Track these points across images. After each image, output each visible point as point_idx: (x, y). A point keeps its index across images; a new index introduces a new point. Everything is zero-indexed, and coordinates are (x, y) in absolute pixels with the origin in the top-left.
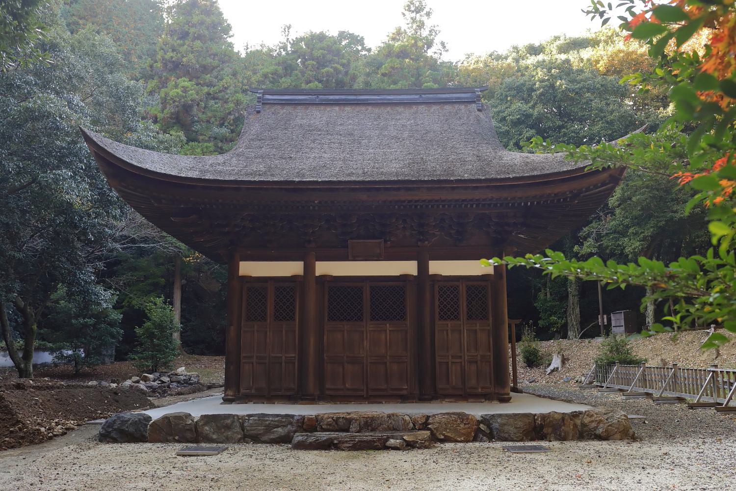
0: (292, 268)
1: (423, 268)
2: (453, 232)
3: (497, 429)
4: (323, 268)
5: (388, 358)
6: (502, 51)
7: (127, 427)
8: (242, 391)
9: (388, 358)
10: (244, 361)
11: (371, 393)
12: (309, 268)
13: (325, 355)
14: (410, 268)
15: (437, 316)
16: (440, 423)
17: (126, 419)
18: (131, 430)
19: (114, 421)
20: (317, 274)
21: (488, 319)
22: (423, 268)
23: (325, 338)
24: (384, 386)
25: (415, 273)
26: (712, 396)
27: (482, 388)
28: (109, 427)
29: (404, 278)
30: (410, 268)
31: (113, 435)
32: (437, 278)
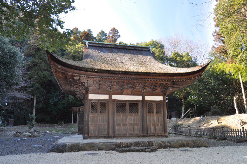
0: (105, 97)
1: (143, 98)
2: (152, 88)
3: (172, 145)
4: (115, 97)
5: (134, 124)
6: (86, 30)
7: (60, 148)
8: (90, 135)
9: (134, 124)
10: (90, 126)
11: (129, 135)
12: (110, 97)
13: (115, 123)
14: (139, 98)
15: (116, 112)
16: (213, 129)
17: (59, 145)
18: (61, 148)
19: (55, 146)
20: (113, 99)
21: (162, 113)
22: (143, 98)
23: (115, 118)
24: (133, 132)
25: (141, 99)
26: (238, 129)
27: (161, 133)
28: (53, 148)
29: (138, 101)
30: (139, 98)
31: (55, 150)
32: (147, 101)
